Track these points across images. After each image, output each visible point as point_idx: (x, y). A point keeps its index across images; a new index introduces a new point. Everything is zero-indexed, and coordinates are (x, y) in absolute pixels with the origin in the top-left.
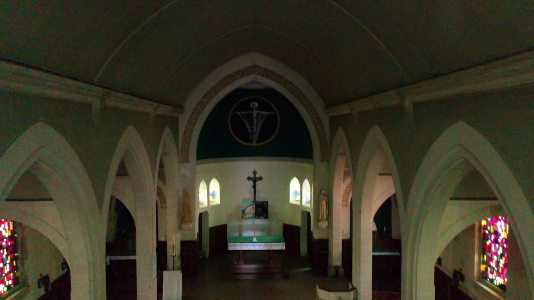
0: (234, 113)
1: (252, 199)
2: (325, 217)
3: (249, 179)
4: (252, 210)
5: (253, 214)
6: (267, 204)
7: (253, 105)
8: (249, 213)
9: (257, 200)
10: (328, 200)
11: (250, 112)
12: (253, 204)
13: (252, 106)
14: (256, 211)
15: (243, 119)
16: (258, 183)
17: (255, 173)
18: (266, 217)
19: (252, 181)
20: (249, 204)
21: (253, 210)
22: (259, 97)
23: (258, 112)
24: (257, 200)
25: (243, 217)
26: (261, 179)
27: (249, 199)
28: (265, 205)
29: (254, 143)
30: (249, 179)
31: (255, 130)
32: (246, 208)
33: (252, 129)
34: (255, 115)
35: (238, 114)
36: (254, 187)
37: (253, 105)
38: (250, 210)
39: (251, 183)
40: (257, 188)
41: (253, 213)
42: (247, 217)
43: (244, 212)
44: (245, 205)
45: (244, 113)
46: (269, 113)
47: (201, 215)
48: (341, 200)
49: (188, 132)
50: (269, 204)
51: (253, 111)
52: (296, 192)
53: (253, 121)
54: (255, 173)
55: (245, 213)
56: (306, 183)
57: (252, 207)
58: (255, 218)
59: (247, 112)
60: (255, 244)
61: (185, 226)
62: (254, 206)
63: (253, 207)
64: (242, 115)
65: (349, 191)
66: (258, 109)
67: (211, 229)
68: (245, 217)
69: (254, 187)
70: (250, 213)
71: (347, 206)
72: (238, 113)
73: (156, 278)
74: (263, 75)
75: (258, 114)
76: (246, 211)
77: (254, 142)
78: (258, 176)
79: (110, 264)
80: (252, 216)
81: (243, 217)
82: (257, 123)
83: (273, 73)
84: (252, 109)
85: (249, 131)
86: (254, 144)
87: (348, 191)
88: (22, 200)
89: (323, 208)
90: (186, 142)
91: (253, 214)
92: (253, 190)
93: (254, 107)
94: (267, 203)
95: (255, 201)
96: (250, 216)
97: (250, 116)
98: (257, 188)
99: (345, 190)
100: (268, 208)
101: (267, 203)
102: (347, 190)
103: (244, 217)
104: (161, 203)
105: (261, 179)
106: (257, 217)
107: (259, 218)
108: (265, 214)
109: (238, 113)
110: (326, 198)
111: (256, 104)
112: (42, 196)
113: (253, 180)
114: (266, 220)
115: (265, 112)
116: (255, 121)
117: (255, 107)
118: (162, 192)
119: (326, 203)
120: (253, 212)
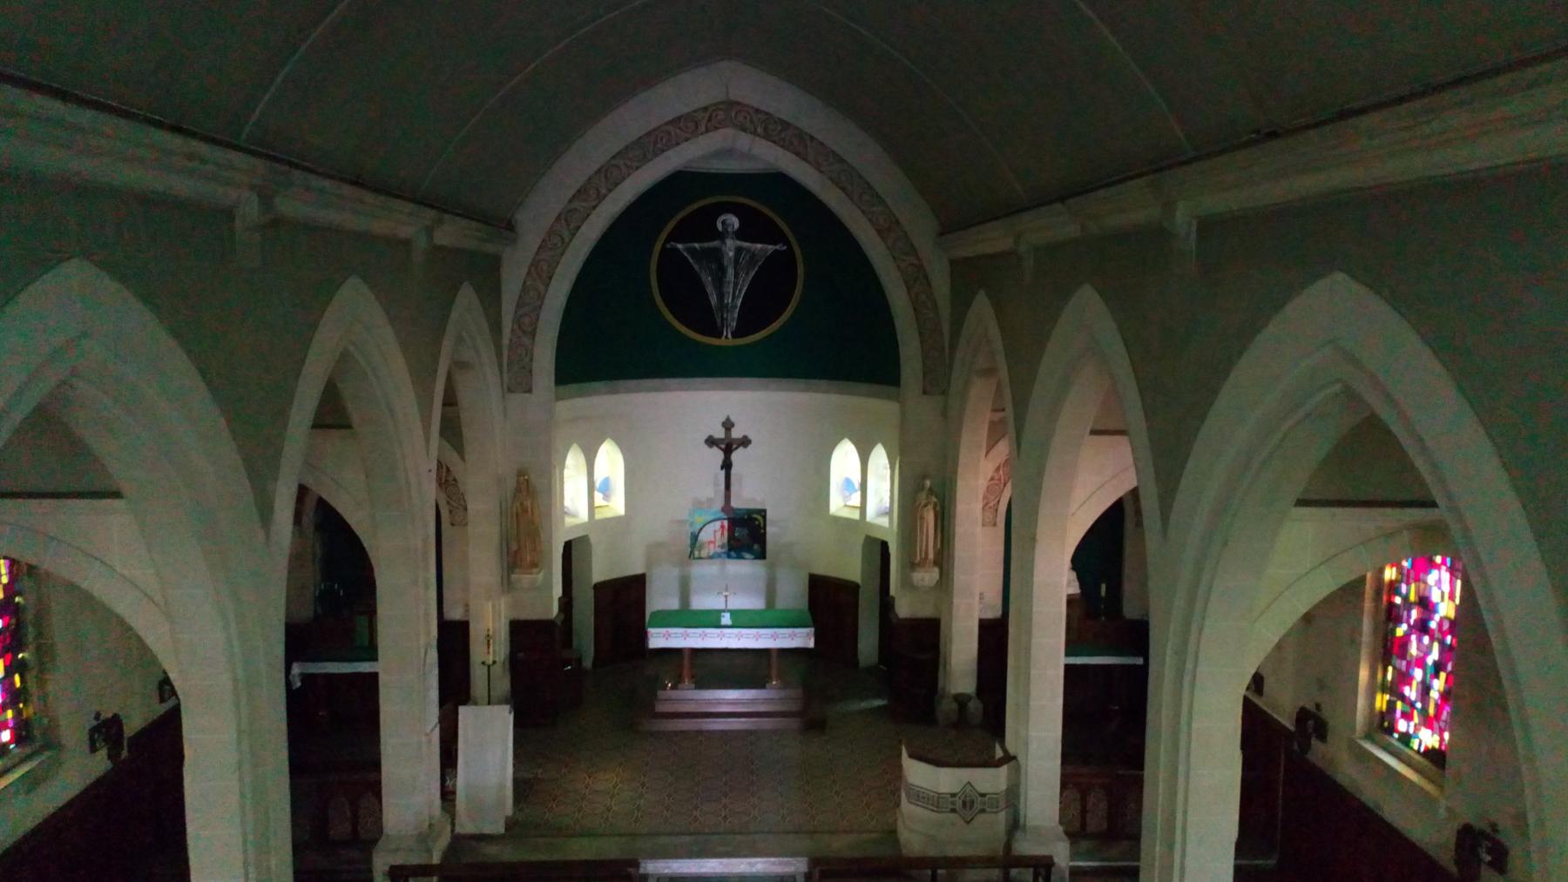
0: (668, 246)
1: (720, 503)
2: (931, 556)
6: (764, 517)
7: (724, 223)
8: (710, 542)
9: (736, 503)
10: (943, 508)
11: (716, 243)
15: (696, 267)
16: (736, 456)
17: (728, 425)
18: (761, 555)
19: (721, 449)
21: (722, 534)
22: (742, 200)
23: (739, 243)
25: (692, 552)
26: (745, 442)
27: (710, 500)
28: (756, 519)
29: (726, 337)
30: (711, 442)
32: (701, 529)
33: (721, 296)
34: (731, 254)
35: (678, 250)
36: (727, 466)
38: (714, 534)
39: (717, 455)
40: (734, 471)
42: (704, 553)
44: (700, 520)
45: (697, 245)
46: (771, 248)
47: (568, 546)
49: (530, 305)
51: (724, 242)
53: (722, 269)
54: (728, 425)
55: (698, 544)
56: (879, 457)
57: (718, 524)
59: (706, 245)
62: (726, 523)
63: (722, 527)
64: (693, 252)
66: (740, 235)
67: (599, 587)
68: (699, 554)
69: (727, 466)
70: (714, 542)
71: (995, 525)
72: (680, 246)
74: (755, 133)
75: (739, 250)
76: (704, 537)
77: (728, 333)
78: (736, 434)
80: (719, 550)
82: (736, 275)
83: (785, 125)
84: (721, 236)
85: (714, 300)
86: (727, 340)
87: (999, 479)
89: (924, 537)
90: (524, 332)
93: (727, 231)
94: (763, 513)
95: (727, 507)
96: (712, 550)
97: (716, 256)
99: (992, 479)
101: (763, 513)
103: (696, 553)
104: (451, 512)
105: (745, 442)
106: (733, 553)
109: (680, 246)
111: (734, 221)
113: (723, 446)
115: (759, 246)
116: (731, 272)
117: (730, 230)
118: (455, 480)
119: (936, 516)
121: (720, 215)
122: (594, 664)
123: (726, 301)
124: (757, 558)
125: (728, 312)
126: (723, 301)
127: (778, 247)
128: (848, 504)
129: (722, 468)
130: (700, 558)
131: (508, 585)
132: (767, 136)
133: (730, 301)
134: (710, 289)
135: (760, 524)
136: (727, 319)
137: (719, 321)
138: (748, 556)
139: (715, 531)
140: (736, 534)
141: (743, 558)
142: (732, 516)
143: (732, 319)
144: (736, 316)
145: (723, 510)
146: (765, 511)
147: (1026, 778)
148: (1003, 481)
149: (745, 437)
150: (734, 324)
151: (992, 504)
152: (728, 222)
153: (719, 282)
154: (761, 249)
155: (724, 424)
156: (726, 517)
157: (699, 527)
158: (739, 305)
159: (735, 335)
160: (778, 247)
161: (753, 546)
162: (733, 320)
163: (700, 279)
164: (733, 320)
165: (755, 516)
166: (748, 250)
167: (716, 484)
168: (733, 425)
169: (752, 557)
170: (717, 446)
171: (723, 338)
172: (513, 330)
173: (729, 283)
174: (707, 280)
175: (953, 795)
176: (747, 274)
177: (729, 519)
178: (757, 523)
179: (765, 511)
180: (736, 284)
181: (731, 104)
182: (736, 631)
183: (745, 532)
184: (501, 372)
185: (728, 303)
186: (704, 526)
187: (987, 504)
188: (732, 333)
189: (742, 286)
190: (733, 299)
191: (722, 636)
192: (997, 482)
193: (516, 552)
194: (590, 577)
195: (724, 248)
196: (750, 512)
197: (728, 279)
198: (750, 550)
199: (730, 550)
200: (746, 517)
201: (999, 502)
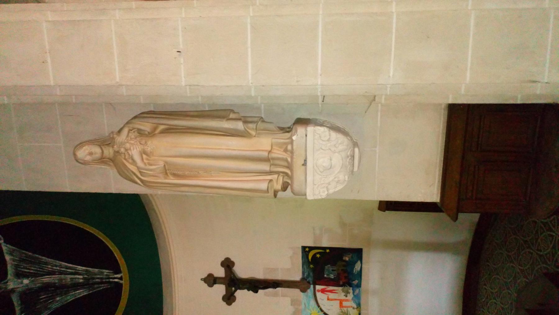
1: (296, 292)
3: (229, 299)
4: (331, 296)
5: (347, 293)
6: (311, 248)
8: (341, 305)
9: (297, 276)
11: (15, 299)
12: (310, 291)
14: (335, 282)
17: (211, 280)
18: (358, 253)
20: (313, 302)
21: (331, 291)
23: (9, 277)
24: (297, 276)
26: (228, 264)
27: (294, 302)
28: (314, 255)
29: (121, 278)
30: (229, 299)
31: (80, 279)
33: (76, 286)
34: (26, 281)
39: (241, 295)
41: (343, 291)
51: (13, 291)
53: (46, 287)
54: (211, 280)
57: (319, 295)
58: (359, 286)
62: (318, 287)
63: (323, 291)
70: (341, 302)
73: (329, 131)
75: (19, 275)
77: (116, 278)
78: (220, 272)
79: (357, 274)
80: (350, 296)
85: (82, 293)
88: (306, 147)
91: (347, 293)
94: (306, 250)
98: (260, 275)
101: (306, 250)
105: (228, 264)
107: (360, 275)
112: (304, 147)
115: (8, 258)
116: (46, 279)
120: (339, 293)
123: (81, 281)
124: (360, 258)
125: (94, 279)
126: (80, 283)
133: (81, 277)
134: (70, 298)
135: (318, 253)
136: (102, 278)
137: (103, 287)
138: (357, 267)
139: (328, 299)
140: (332, 276)
141: (360, 273)
142: (310, 279)
144: (96, 270)
145: (304, 290)
146: (304, 248)
149: (223, 264)
150: (106, 272)
153: (63, 288)
154: (11, 254)
155: (211, 285)
156: (312, 286)
159: (118, 271)
161: (345, 261)
162: (102, 273)
163: (57, 309)
164: (103, 273)
165: (310, 258)
166: (17, 267)
168: (210, 276)
169: (359, 262)
171: (121, 282)
173: (61, 280)
174: (59, 301)
176: (46, 263)
177: (315, 284)
178: (318, 256)
179: (304, 248)
180: (61, 273)
185: (84, 278)
186: (322, 310)
189: (61, 266)
190: (80, 274)
195: (20, 290)
196: (306, 261)
197: (57, 281)
198: (353, 264)
199: (350, 285)
200: (312, 266)
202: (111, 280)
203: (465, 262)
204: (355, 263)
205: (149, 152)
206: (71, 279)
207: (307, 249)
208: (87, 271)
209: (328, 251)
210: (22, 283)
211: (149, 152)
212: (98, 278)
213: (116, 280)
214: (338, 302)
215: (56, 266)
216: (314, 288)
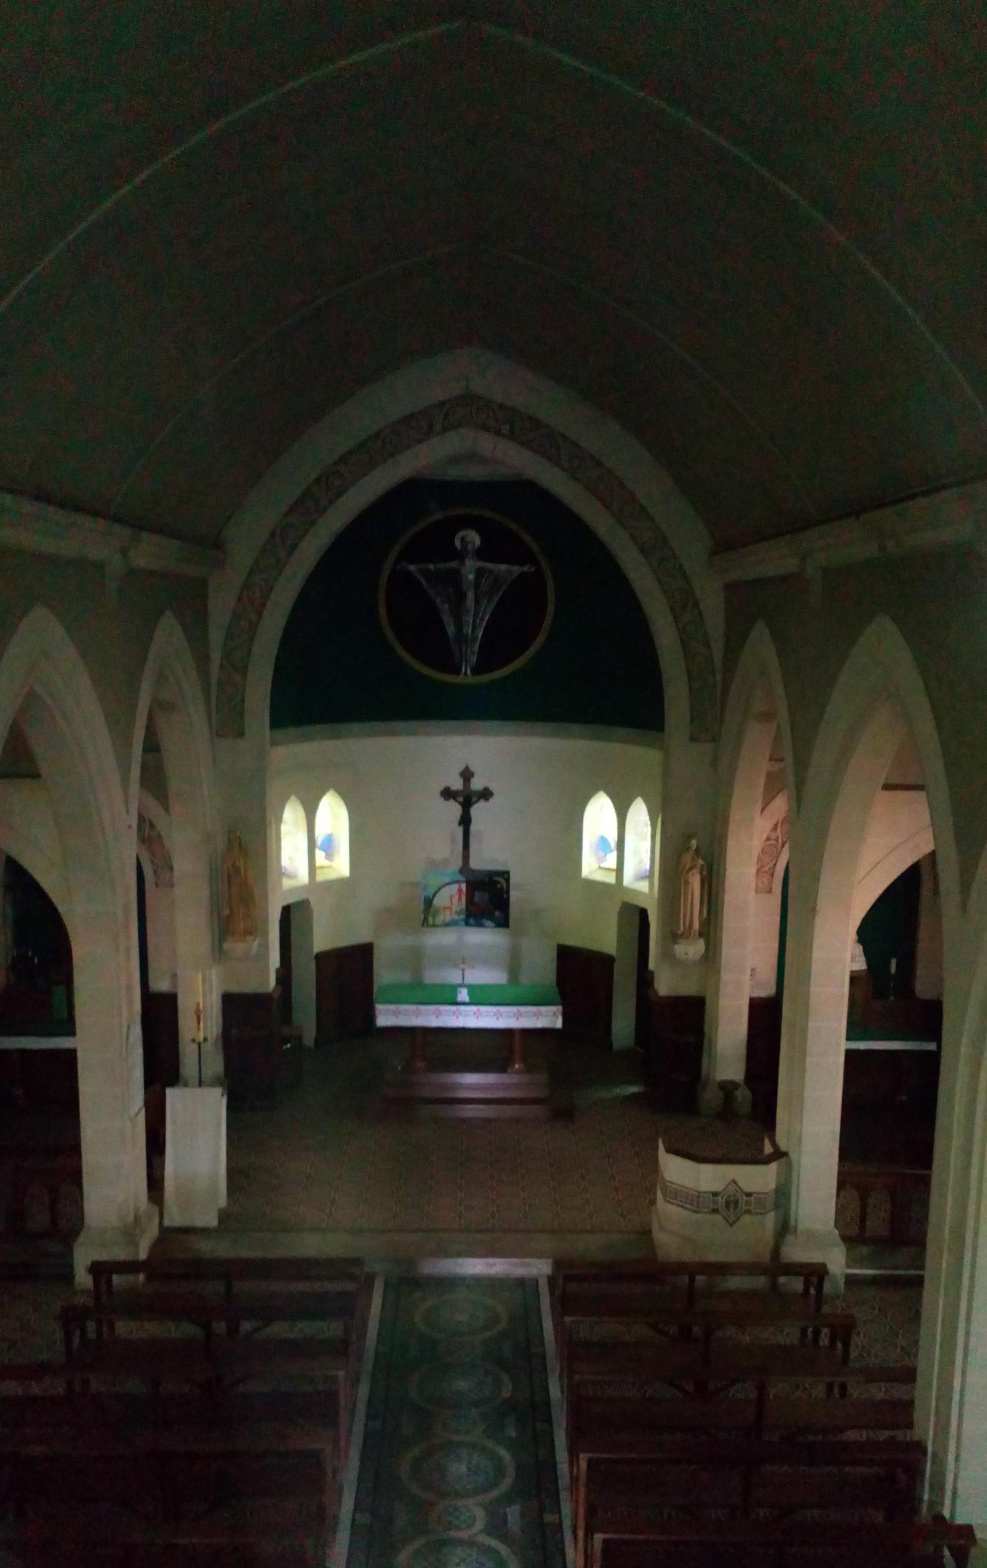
1: (459, 863)
5: (459, 913)
6: (508, 880)
7: (463, 539)
8: (445, 908)
9: (475, 864)
10: (710, 870)
11: (453, 564)
13: (457, 543)
16: (477, 810)
17: (467, 775)
18: (504, 923)
20: (448, 880)
23: (480, 564)
24: (475, 864)
25: (425, 920)
26: (486, 794)
27: (445, 862)
28: (498, 882)
30: (447, 794)
33: (459, 626)
36: (465, 821)
37: (463, 539)
39: (454, 809)
40: (473, 828)
41: (461, 910)
42: (439, 920)
43: (429, 902)
44: (434, 882)
45: (432, 567)
46: (516, 569)
48: (751, 871)
50: (512, 881)
51: (463, 563)
52: (603, 841)
53: (462, 596)
54: (467, 775)
55: (432, 909)
56: (639, 813)
59: (441, 566)
60: (462, 1008)
61: (235, 947)
62: (464, 886)
63: (460, 890)
64: (426, 573)
65: (780, 841)
66: (481, 554)
69: (465, 821)
70: (450, 908)
71: (770, 891)
72: (412, 568)
74: (498, 433)
75: (480, 573)
77: (467, 669)
78: (477, 784)
80: (456, 917)
81: (425, 920)
82: (477, 602)
83: (536, 423)
84: (460, 556)
85: (451, 630)
86: (466, 677)
87: (777, 840)
89: (690, 896)
91: (459, 913)
92: (460, 831)
93: (466, 548)
94: (506, 875)
95: (465, 868)
97: (454, 578)
99: (768, 839)
100: (508, 892)
101: (506, 875)
102: (773, 836)
103: (430, 920)
104: (155, 872)
105: (486, 794)
106: (471, 921)
107: (480, 925)
108: (497, 913)
109: (412, 568)
110: (701, 862)
111: (474, 539)
113: (461, 799)
114: (502, 930)
115: (503, 567)
116: (471, 596)
117: (470, 547)
121: (457, 532)
122: (316, 1041)
123: (465, 631)
127: (525, 568)
128: (603, 865)
129: (460, 824)
130: (434, 926)
131: (219, 953)
132: (512, 437)
133: (470, 631)
135: (502, 886)
139: (451, 897)
140: (476, 899)
143: (472, 654)
144: (476, 649)
145: (461, 871)
146: (508, 873)
147: (798, 1194)
148: (780, 841)
150: (474, 659)
151: (766, 868)
152: (468, 539)
157: (433, 892)
158: (480, 636)
159: (476, 671)
160: (525, 568)
165: (496, 878)
166: (491, 572)
167: (453, 841)
168: (472, 775)
170: (455, 799)
172: (221, 666)
174: (444, 607)
175: (715, 1194)
179: (508, 873)
181: (468, 399)
182: (474, 1008)
183: (486, 896)
184: (210, 719)
185: (467, 634)
187: (762, 867)
188: (472, 670)
189: (484, 613)
191: (458, 1014)
192: (773, 842)
193: (228, 918)
194: (311, 947)
195: (462, 572)
201: (775, 865)
202: (464, 663)
203: (375, 978)
204: (492, 920)
205: (826, 1294)
206: (468, 622)
207: (506, 876)
208: (477, 638)
209: (505, 896)
210: (471, 572)
211: (826, 1294)
212: (466, 651)
213: (463, 670)
214: (450, 905)
215: (485, 609)
216: (463, 882)
